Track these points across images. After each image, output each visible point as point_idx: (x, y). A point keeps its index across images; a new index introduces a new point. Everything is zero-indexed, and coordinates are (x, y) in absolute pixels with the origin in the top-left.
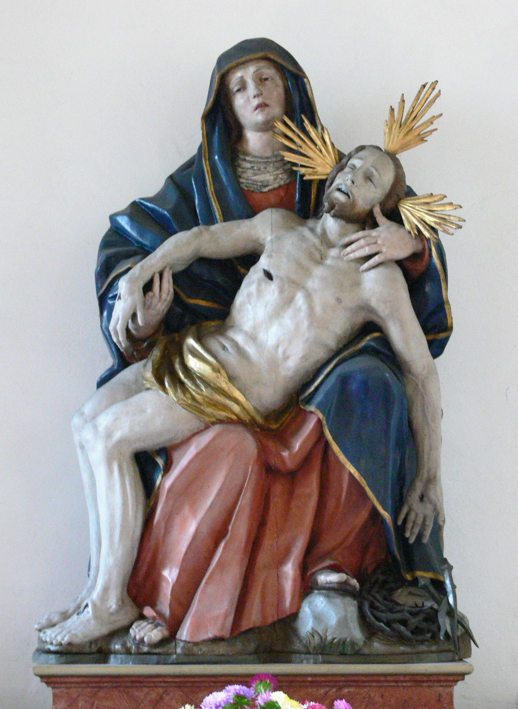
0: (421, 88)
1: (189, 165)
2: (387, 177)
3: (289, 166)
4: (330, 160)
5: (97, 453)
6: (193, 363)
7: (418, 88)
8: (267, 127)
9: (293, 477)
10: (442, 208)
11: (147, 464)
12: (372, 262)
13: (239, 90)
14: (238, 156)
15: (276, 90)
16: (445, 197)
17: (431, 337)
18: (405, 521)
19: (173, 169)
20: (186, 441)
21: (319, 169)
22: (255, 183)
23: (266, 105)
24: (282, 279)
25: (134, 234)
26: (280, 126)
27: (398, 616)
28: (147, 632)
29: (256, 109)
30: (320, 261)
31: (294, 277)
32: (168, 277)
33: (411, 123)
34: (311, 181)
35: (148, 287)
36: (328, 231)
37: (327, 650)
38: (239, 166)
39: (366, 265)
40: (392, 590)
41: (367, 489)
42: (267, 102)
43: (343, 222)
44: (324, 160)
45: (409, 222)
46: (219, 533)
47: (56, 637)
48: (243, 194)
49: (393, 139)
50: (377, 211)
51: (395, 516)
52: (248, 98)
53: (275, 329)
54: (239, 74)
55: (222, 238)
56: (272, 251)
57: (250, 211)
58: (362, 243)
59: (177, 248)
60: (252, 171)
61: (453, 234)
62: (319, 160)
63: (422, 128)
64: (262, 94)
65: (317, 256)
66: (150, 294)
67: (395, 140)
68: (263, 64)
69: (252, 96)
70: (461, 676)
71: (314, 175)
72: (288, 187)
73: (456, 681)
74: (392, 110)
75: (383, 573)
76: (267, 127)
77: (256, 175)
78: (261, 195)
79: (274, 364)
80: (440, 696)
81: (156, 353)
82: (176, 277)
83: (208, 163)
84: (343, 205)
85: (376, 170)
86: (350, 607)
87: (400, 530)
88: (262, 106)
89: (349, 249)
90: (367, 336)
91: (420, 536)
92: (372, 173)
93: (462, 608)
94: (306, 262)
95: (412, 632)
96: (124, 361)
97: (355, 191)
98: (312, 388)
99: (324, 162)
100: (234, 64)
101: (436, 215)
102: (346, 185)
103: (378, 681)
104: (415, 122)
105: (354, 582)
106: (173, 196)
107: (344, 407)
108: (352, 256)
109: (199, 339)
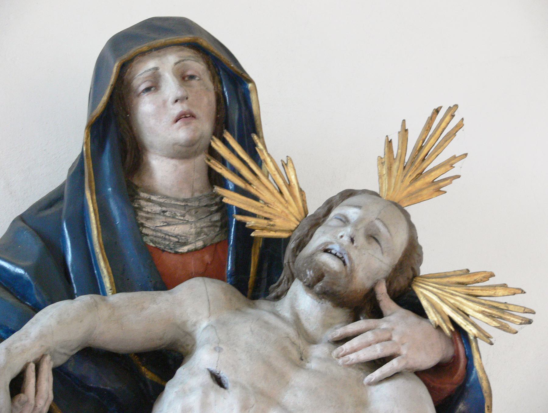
0: (433, 113)
1: (53, 200)
4: (296, 209)
7: (429, 114)
8: (183, 153)
10: (491, 293)
12: (386, 369)
13: (148, 89)
14: (138, 194)
16: (492, 275)
21: (278, 222)
22: (167, 237)
23: (193, 116)
24: (243, 388)
29: (176, 121)
31: (262, 385)
33: (419, 163)
36: (303, 317)
38: (140, 208)
39: (378, 374)
42: (195, 111)
43: (328, 304)
44: (287, 208)
45: (438, 311)
48: (150, 254)
49: (395, 184)
50: (382, 290)
52: (165, 102)
54: (151, 64)
56: (219, 341)
57: (164, 282)
58: (366, 340)
60: (163, 218)
61: (516, 332)
62: (279, 208)
63: (438, 172)
64: (187, 98)
65: (295, 355)
66: (22, 397)
67: (398, 187)
68: (188, 53)
69: (171, 99)
71: (271, 230)
72: (215, 248)
76: (183, 153)
77: (168, 224)
78: (175, 257)
82: (59, 373)
83: (94, 197)
84: (335, 274)
85: (385, 225)
88: (185, 117)
89: (347, 346)
92: (378, 229)
94: (280, 364)
97: (354, 254)
99: (287, 212)
100: (144, 47)
101: (483, 301)
102: (341, 245)
104: (424, 165)
106: (33, 246)
108: (353, 357)
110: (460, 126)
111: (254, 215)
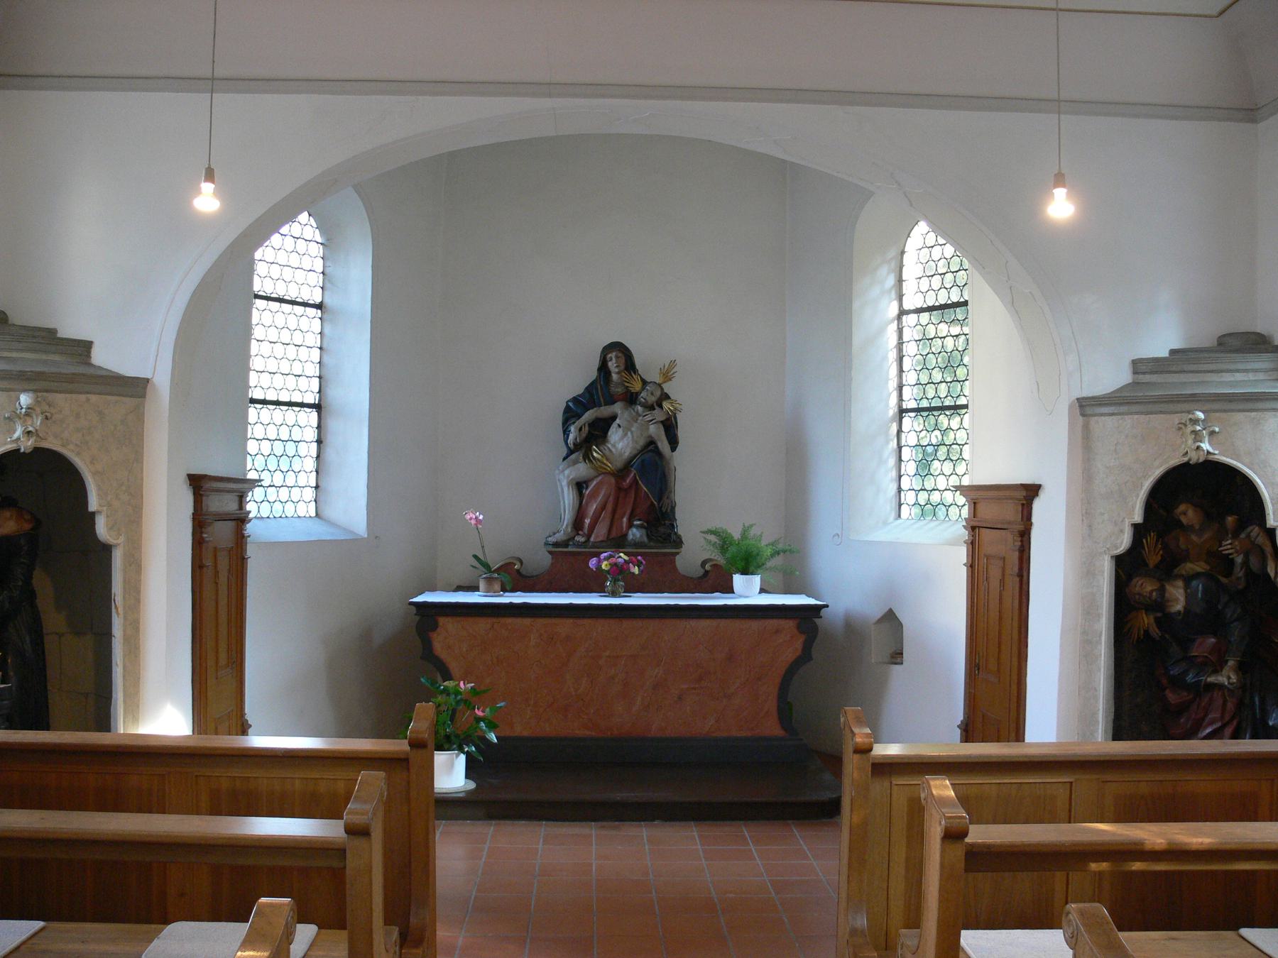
2: (658, 393)
5: (564, 483)
8: (618, 373)
9: (627, 491)
11: (580, 486)
20: (592, 479)
28: (580, 539)
30: (636, 421)
33: (667, 375)
35: (580, 429)
37: (637, 544)
46: (603, 507)
47: (551, 540)
53: (621, 443)
55: (605, 411)
57: (613, 403)
59: (589, 416)
76: (618, 373)
79: (621, 455)
86: (644, 531)
90: (651, 444)
93: (680, 532)
96: (571, 452)
107: (643, 469)
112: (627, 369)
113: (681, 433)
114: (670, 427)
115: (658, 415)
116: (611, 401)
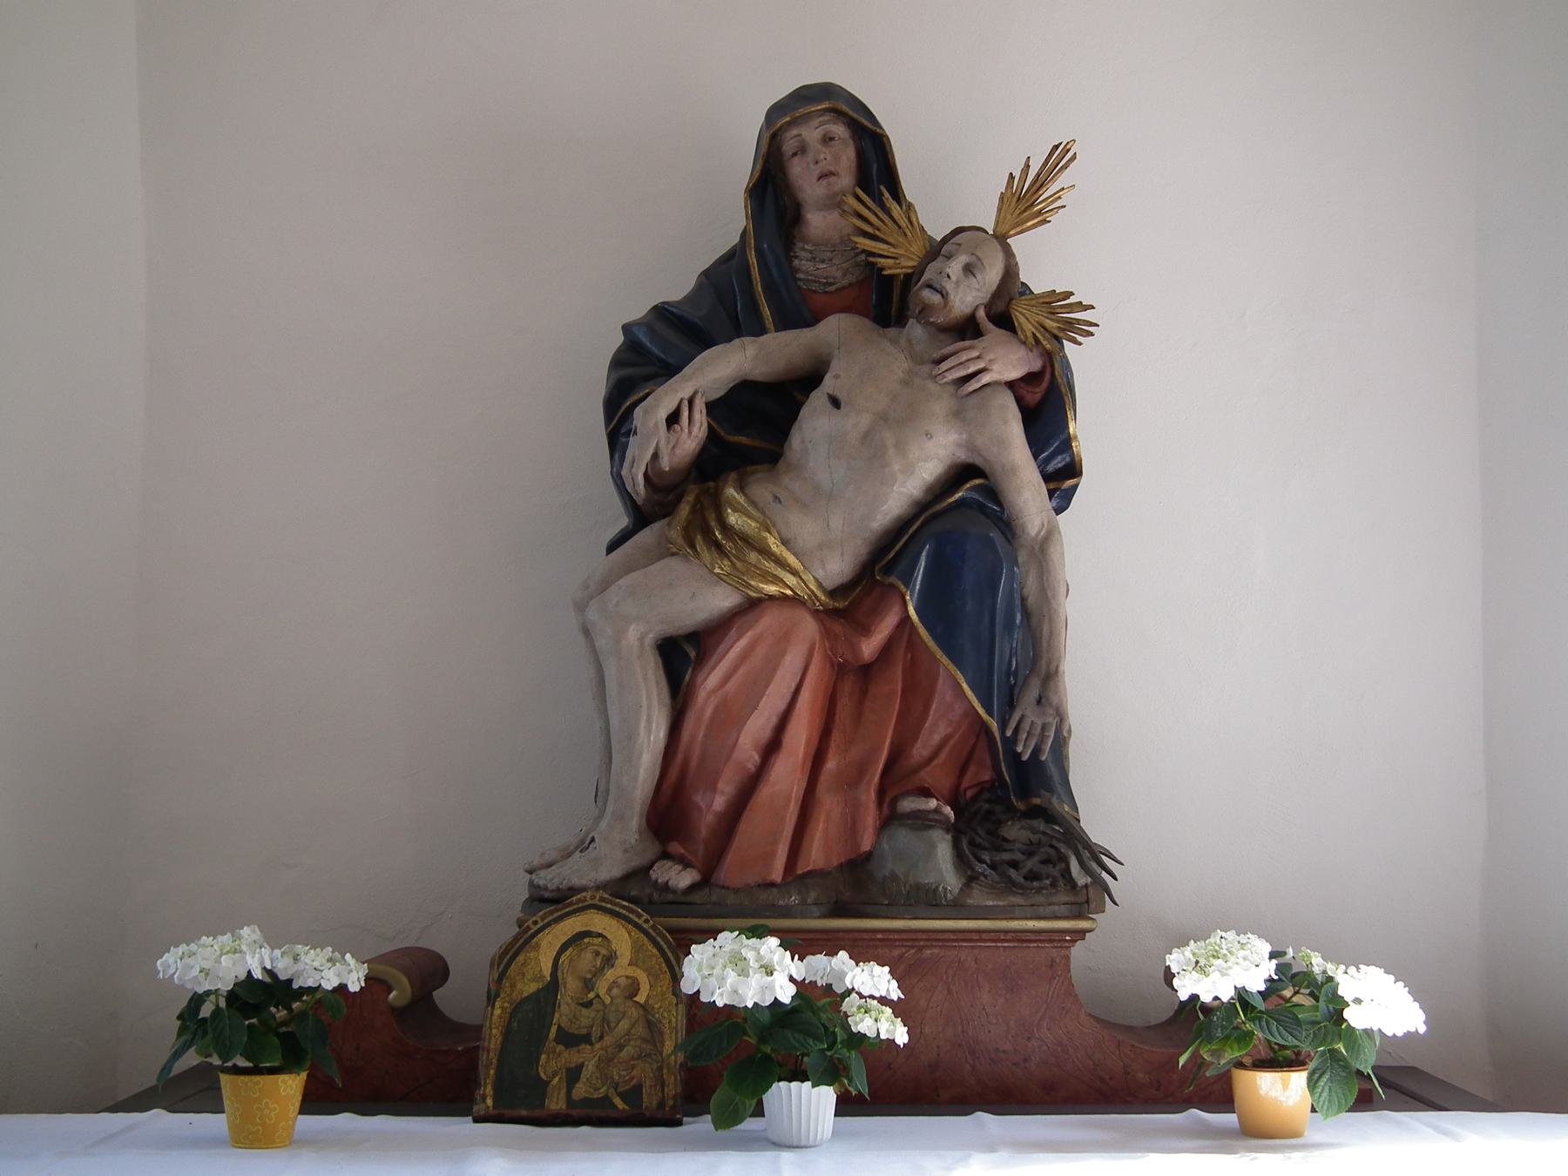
1: (730, 256)
2: (992, 275)
3: (863, 257)
6: (733, 519)
11: (681, 656)
15: (846, 157)
17: (1052, 486)
18: (1017, 730)
19: (706, 263)
25: (656, 351)
26: (852, 201)
27: (1006, 856)
32: (700, 405)
33: (1026, 201)
34: (892, 277)
40: (999, 823)
41: (965, 686)
50: (981, 314)
51: (1003, 726)
59: (720, 367)
70: (1081, 934)
73: (1074, 941)
74: (1011, 176)
75: (988, 801)
80: (1053, 960)
81: (684, 510)
82: (711, 407)
87: (1010, 743)
89: (944, 366)
91: (1037, 751)
95: (1026, 878)
96: (641, 517)
98: (892, 554)
103: (970, 940)
105: (948, 810)
109: (741, 488)
110: (1074, 158)
111: (881, 256)
112: (864, 180)
113: (1088, 428)
114: (1045, 407)
115: (1007, 362)
116: (797, 312)
